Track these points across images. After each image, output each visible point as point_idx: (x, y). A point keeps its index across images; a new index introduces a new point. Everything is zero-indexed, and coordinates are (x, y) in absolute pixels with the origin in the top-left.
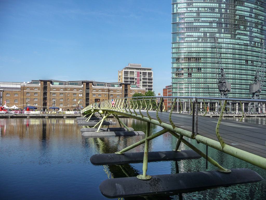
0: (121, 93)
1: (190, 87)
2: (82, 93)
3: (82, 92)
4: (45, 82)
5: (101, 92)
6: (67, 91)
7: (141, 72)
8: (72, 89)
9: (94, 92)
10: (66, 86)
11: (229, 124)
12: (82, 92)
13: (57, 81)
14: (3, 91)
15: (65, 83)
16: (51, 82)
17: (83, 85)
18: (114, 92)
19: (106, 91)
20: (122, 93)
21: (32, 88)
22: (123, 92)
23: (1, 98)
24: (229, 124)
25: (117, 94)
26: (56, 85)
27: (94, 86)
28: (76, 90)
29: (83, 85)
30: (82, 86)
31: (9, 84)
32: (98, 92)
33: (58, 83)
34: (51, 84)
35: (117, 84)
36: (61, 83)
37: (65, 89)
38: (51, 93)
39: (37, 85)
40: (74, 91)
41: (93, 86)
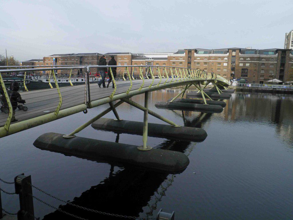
0: (276, 62)
1: (60, 96)
2: (228, 63)
4: (190, 51)
6: (211, 60)
8: (216, 58)
9: (86, 60)
13: (201, 50)
15: (210, 52)
16: (196, 51)
18: (176, 60)
19: (256, 59)
20: (277, 61)
21: (177, 58)
22: (279, 61)
24: (245, 56)
25: (271, 63)
26: (201, 55)
27: (241, 54)
28: (199, 59)
29: (185, 53)
31: (164, 55)
32: (50, 61)
34: (195, 53)
35: (272, 51)
36: (206, 52)
37: (209, 58)
38: (195, 62)
39: (182, 54)
40: (218, 60)
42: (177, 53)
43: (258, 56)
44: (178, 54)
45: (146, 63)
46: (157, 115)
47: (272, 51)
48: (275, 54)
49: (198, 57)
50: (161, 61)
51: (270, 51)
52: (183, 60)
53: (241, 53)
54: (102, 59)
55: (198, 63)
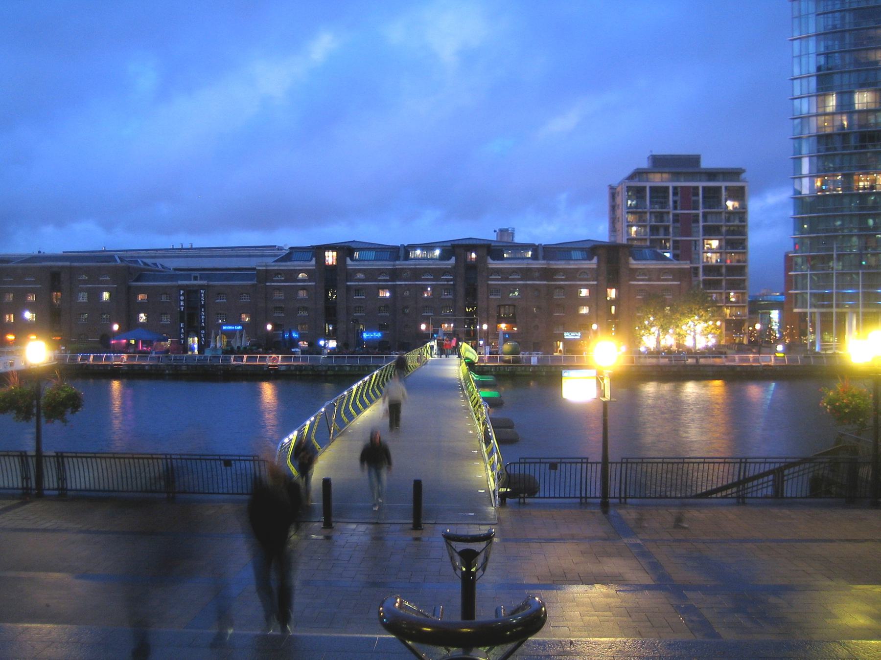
0: (595, 283)
3: (452, 283)
5: (672, 280)
7: (697, 188)
10: (397, 262)
11: (429, 265)
12: (452, 283)
14: (208, 286)
17: (454, 258)
19: (537, 274)
23: (203, 310)
24: (429, 265)
29: (454, 258)
30: (453, 261)
32: (507, 279)
33: (372, 255)
35: (582, 249)
41: (490, 261)
42: (161, 265)
43: (544, 264)
44: (286, 261)
45: (182, 292)
46: (310, 471)
47: (582, 249)
48: (590, 258)
49: (360, 271)
50: (234, 286)
51: (575, 249)
52: (309, 280)
53: (491, 258)
54: (744, 503)
55: (358, 290)
